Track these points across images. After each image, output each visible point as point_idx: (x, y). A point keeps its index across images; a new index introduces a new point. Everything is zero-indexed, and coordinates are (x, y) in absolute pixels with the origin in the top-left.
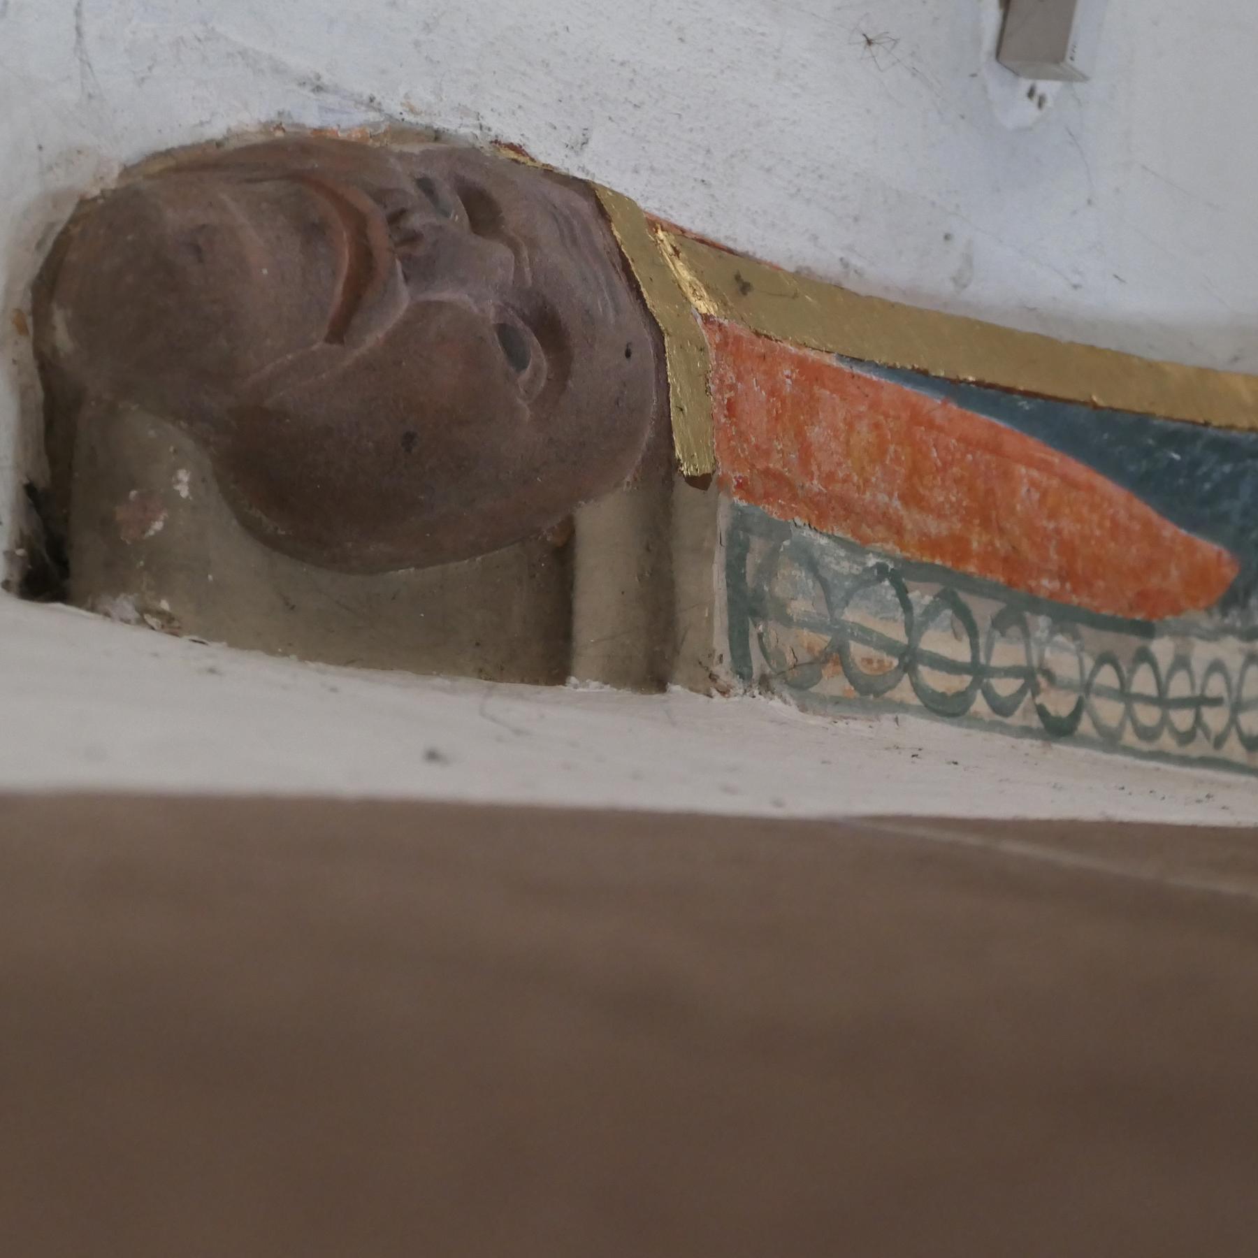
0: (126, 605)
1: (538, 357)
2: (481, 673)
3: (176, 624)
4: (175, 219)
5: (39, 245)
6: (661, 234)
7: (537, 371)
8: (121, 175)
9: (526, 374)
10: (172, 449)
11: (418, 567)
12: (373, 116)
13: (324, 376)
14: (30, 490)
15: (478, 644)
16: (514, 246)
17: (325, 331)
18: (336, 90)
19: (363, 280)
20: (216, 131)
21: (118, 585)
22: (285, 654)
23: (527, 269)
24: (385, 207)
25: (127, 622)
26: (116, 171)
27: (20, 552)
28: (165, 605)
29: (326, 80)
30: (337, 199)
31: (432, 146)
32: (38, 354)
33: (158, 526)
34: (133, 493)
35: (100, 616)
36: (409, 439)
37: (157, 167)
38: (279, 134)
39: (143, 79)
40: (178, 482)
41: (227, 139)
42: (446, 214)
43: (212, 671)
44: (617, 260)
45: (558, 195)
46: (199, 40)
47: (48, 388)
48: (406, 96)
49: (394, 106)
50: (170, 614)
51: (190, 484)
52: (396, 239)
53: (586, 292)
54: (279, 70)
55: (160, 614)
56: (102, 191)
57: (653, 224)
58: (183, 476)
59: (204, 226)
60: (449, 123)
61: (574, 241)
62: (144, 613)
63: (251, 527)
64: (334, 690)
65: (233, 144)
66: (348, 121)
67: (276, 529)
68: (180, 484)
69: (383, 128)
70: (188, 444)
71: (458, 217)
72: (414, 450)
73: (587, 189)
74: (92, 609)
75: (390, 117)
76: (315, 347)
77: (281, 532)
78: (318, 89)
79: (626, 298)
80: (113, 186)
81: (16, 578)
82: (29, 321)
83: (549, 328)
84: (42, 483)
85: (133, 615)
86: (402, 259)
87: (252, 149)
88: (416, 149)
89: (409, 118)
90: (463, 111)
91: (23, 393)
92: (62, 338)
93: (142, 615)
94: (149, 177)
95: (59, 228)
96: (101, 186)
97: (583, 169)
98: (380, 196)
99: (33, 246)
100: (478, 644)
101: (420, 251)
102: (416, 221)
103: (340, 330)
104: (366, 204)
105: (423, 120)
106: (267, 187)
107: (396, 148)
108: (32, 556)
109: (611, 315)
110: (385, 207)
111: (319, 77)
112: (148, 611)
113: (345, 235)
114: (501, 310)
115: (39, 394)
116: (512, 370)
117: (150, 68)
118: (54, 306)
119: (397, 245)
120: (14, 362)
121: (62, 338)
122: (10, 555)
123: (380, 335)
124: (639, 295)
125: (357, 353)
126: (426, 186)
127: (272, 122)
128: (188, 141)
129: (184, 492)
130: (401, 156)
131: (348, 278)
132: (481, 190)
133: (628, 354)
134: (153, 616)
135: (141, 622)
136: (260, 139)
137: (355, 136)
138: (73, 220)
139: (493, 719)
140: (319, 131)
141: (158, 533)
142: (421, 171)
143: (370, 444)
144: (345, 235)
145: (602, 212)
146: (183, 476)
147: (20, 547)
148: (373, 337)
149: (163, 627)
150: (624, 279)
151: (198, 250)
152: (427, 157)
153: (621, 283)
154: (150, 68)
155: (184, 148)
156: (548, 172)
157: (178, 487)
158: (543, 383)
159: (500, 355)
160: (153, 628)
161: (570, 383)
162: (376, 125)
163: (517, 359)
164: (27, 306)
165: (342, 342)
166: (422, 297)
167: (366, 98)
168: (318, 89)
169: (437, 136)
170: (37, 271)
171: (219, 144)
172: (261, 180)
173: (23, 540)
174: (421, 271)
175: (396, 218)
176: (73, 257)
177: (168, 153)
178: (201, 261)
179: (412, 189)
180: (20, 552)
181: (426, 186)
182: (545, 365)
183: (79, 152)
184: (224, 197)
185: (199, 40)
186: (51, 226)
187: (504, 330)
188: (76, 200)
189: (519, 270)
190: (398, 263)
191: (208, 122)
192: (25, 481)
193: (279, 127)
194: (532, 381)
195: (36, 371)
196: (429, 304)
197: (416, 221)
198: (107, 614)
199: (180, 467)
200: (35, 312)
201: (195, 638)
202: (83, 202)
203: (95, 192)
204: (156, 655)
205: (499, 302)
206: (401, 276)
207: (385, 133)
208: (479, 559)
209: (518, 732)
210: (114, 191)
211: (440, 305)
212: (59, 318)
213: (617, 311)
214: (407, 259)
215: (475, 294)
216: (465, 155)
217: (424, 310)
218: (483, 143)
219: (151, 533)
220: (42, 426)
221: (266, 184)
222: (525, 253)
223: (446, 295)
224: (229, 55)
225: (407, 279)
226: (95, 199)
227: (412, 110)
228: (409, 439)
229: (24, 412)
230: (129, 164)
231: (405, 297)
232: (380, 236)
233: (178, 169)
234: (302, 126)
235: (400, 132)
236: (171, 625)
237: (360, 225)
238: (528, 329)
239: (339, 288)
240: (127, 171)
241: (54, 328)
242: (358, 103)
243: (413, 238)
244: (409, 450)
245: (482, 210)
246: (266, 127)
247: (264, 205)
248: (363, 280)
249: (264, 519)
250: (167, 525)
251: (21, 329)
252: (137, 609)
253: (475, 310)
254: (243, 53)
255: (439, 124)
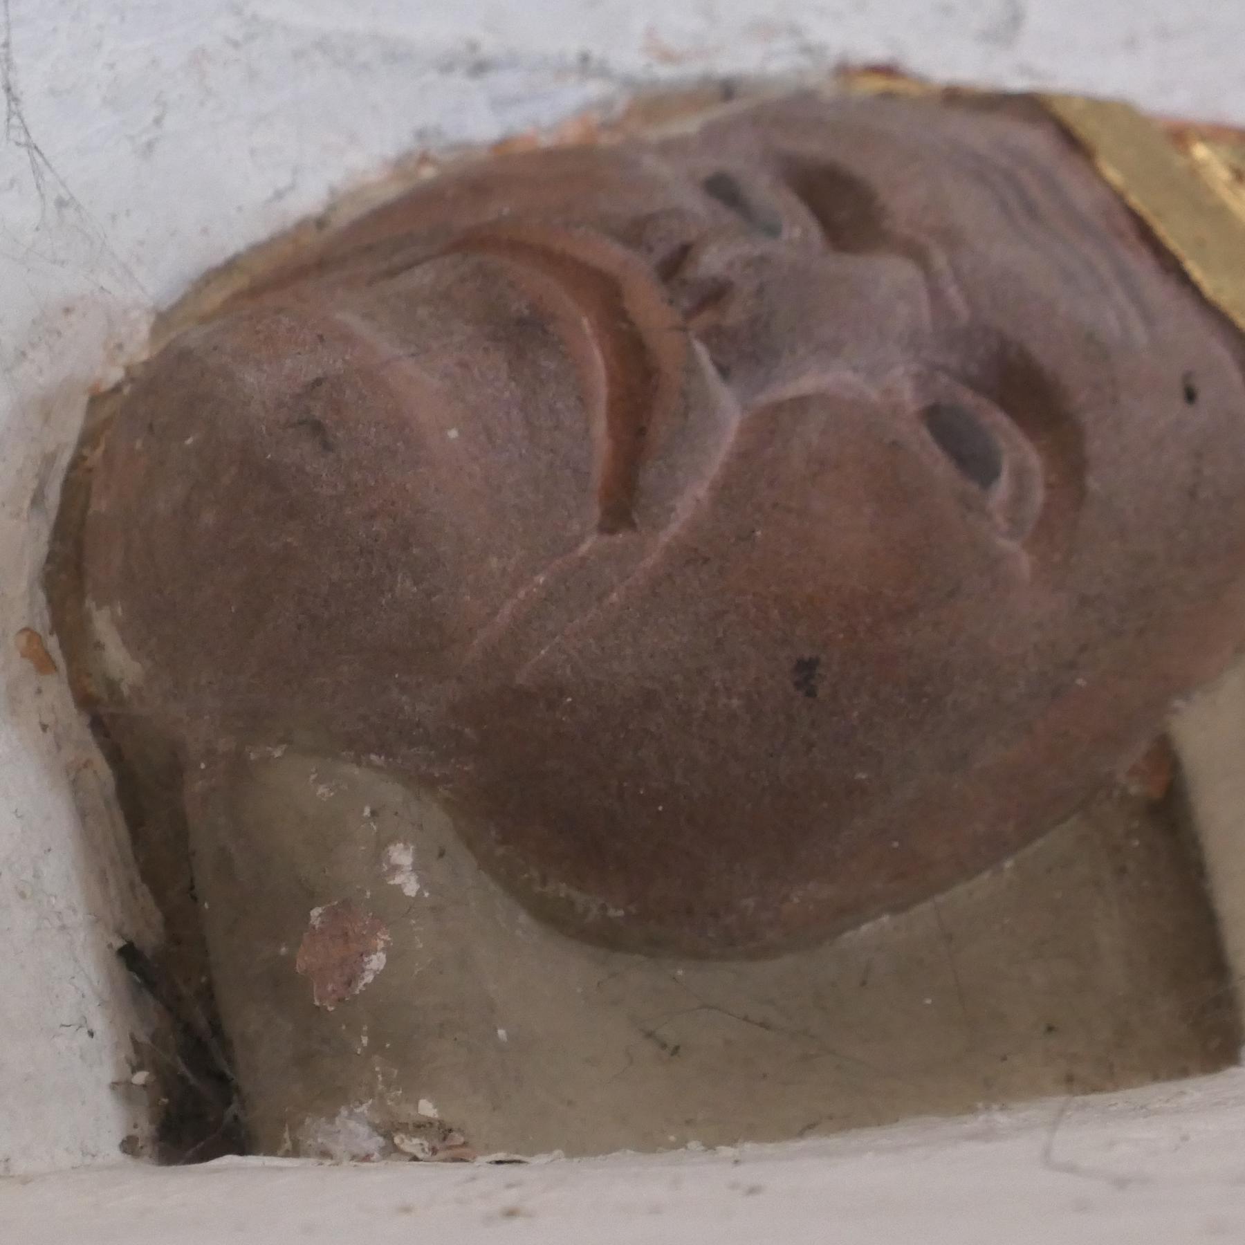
0: (354, 1127)
1: (1018, 450)
2: (1071, 1083)
3: (458, 1139)
4: (261, 383)
5: (37, 500)
6: (1201, 152)
7: (1020, 474)
8: (155, 331)
9: (1003, 488)
10: (367, 811)
11: (895, 910)
12: (594, 89)
13: (614, 597)
14: (129, 955)
15: (1050, 1029)
16: (916, 253)
17: (595, 513)
18: (512, 61)
19: (640, 391)
20: (308, 199)
21: (331, 1096)
22: (682, 1144)
23: (952, 291)
24: (650, 250)
25: (367, 1158)
26: (144, 330)
27: (140, 1078)
28: (427, 1109)
29: (490, 46)
30: (553, 260)
31: (719, 112)
32: (85, 701)
33: (377, 962)
34: (316, 912)
35: (312, 1161)
36: (806, 670)
37: (216, 297)
38: (428, 173)
39: (150, 146)
40: (396, 868)
41: (332, 208)
42: (773, 231)
43: (511, 1213)
44: (1124, 223)
45: (978, 133)
46: (236, 45)
47: (115, 757)
48: (651, 33)
49: (631, 60)
50: (441, 1123)
51: (416, 868)
52: (686, 303)
53: (1077, 302)
54: (396, 55)
55: (421, 1127)
56: (128, 369)
57: (1180, 135)
58: (402, 855)
59: (318, 382)
60: (743, 59)
61: (1031, 210)
62: (390, 1135)
63: (556, 919)
64: (753, 1191)
65: (341, 220)
66: (549, 111)
67: (604, 908)
68: (398, 872)
69: (621, 106)
70: (393, 793)
71: (799, 228)
72: (823, 691)
73: (1033, 107)
74: (295, 1151)
75: (628, 82)
76: (584, 548)
77: (616, 913)
78: (480, 68)
79: (1158, 290)
80: (144, 356)
81: (146, 1129)
82: (52, 643)
83: (1025, 388)
84: (151, 939)
85: (374, 1143)
86: (706, 337)
87: (383, 214)
88: (689, 126)
89: (665, 72)
90: (763, 30)
91: (75, 781)
92: (119, 660)
93: (388, 1136)
94: (204, 319)
95: (65, 459)
96: (123, 360)
97: (1025, 70)
98: (635, 233)
99: (27, 503)
100: (1050, 1029)
101: (735, 315)
102: (713, 261)
103: (623, 503)
104: (610, 255)
105: (693, 69)
106: (422, 277)
107: (653, 134)
108: (165, 1080)
109: (1140, 333)
110: (650, 250)
111: (473, 47)
112: (402, 1127)
113: (585, 322)
114: (922, 381)
115: (102, 773)
116: (973, 488)
117: (158, 121)
118: (90, 603)
119: (689, 315)
120: (44, 728)
121: (119, 660)
122: (122, 1088)
123: (700, 491)
124: (1184, 279)
125: (664, 538)
126: (722, 189)
127: (409, 154)
128: (261, 232)
129: (411, 887)
130: (667, 148)
131: (612, 404)
132: (835, 166)
133: (1190, 396)
134: (412, 1135)
135: (391, 1151)
136: (393, 191)
137: (572, 135)
138: (88, 438)
139: (1071, 1169)
140: (502, 148)
141: (379, 977)
142: (708, 164)
143: (735, 702)
144: (585, 322)
145: (1073, 142)
146: (402, 855)
147: (134, 1070)
148: (688, 497)
149: (434, 1151)
150: (1145, 252)
151: (317, 428)
152: (713, 136)
153: (1142, 265)
154: (158, 121)
155: (258, 249)
156: (954, 98)
157: (398, 880)
158: (1038, 496)
159: (940, 466)
160: (415, 1159)
161: (1093, 483)
162: (605, 104)
163: (976, 463)
164: (42, 620)
165: (632, 525)
166: (763, 399)
167: (572, 58)
168: (480, 68)
169: (728, 90)
170: (43, 550)
171: (320, 223)
172: (409, 266)
173: (140, 1056)
174: (746, 351)
175: (673, 267)
176: (100, 505)
177: (231, 266)
178: (327, 447)
179: (696, 204)
180: (140, 1078)
181: (722, 189)
182: (1035, 461)
183: (67, 311)
184: (350, 319)
185: (236, 45)
186: (49, 460)
187: (941, 421)
188: (84, 400)
189: (936, 294)
190: (700, 349)
191: (292, 187)
192: (119, 943)
193: (424, 159)
194: (1019, 497)
195: (88, 736)
196: (778, 407)
197: (713, 261)
198: (325, 1154)
199: (392, 840)
200: (58, 626)
201: (501, 1156)
202: (97, 399)
203: (116, 374)
204: (407, 1210)
205: (914, 368)
206: (710, 371)
207: (629, 114)
208: (1008, 864)
209: (1121, 1183)
210: (146, 364)
211: (801, 404)
212: (104, 624)
213: (1149, 319)
214: (715, 336)
215: (867, 361)
216: (787, 111)
217: (771, 424)
218: (818, 78)
219: (361, 985)
220: (123, 832)
221: (418, 271)
222: (940, 260)
223: (807, 384)
224: (298, 55)
225: (724, 372)
226: (117, 389)
227: (667, 57)
228: (806, 670)
229: (82, 814)
230: (164, 307)
231: (729, 409)
232: (650, 307)
233: (254, 292)
234: (466, 146)
235: (654, 103)
236: (447, 1143)
237: (607, 295)
238: (984, 402)
239: (600, 427)
240: (163, 320)
241: (99, 646)
242: (561, 72)
243: (716, 294)
244: (811, 693)
245: (840, 204)
246: (400, 166)
247: (423, 312)
248: (640, 391)
249: (575, 894)
250: (393, 956)
251: (44, 664)
252: (375, 1128)
253: (874, 395)
254: (322, 44)
255: (726, 65)
